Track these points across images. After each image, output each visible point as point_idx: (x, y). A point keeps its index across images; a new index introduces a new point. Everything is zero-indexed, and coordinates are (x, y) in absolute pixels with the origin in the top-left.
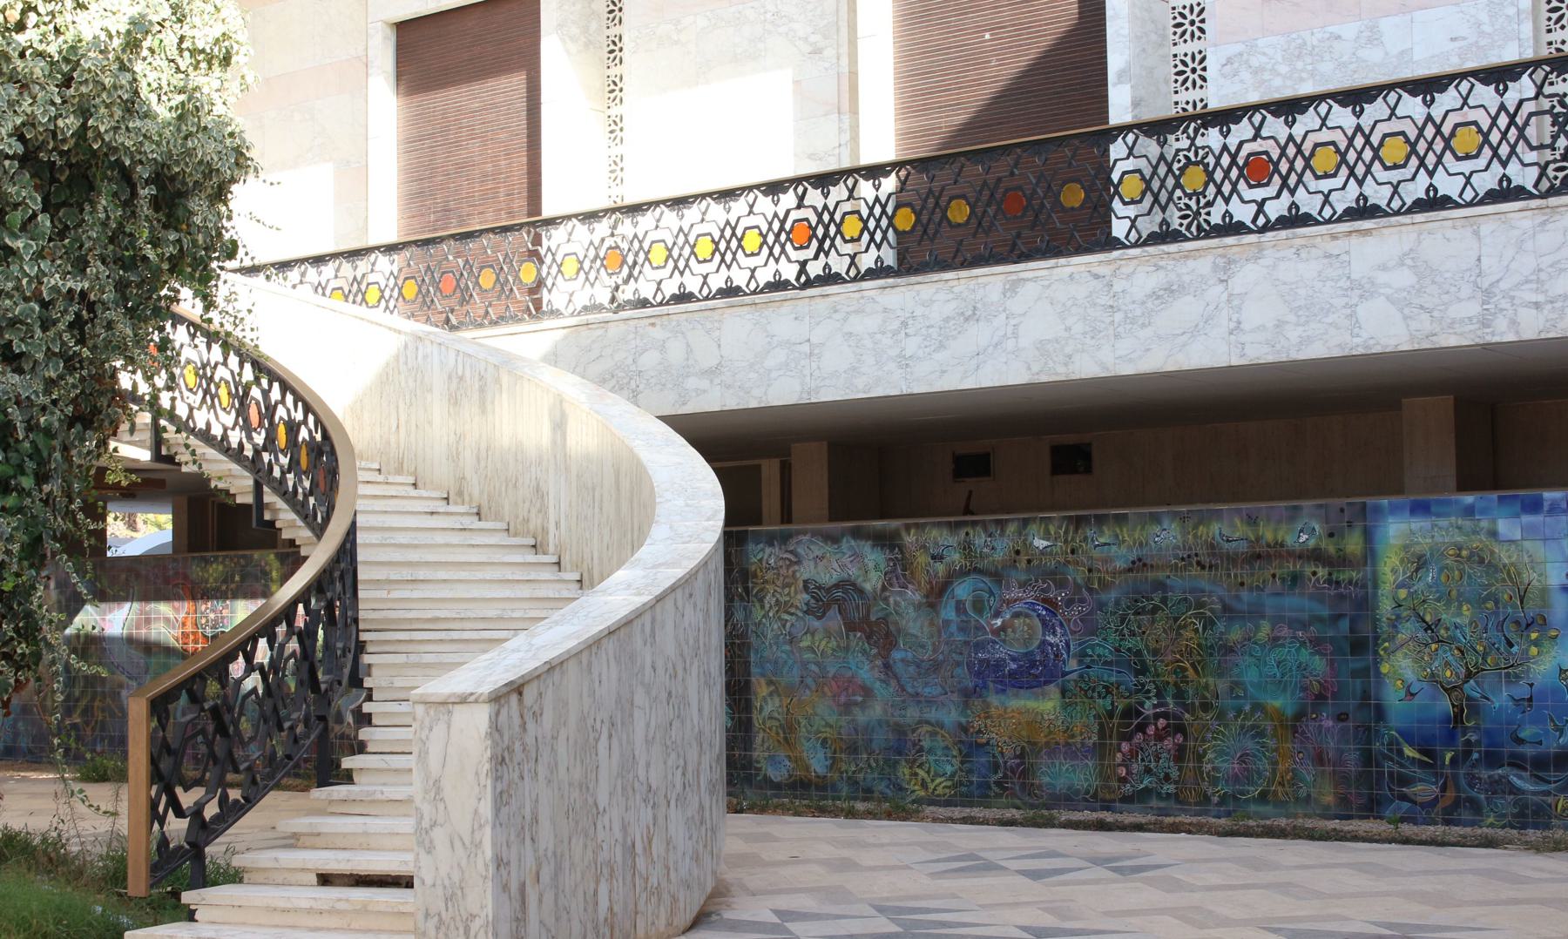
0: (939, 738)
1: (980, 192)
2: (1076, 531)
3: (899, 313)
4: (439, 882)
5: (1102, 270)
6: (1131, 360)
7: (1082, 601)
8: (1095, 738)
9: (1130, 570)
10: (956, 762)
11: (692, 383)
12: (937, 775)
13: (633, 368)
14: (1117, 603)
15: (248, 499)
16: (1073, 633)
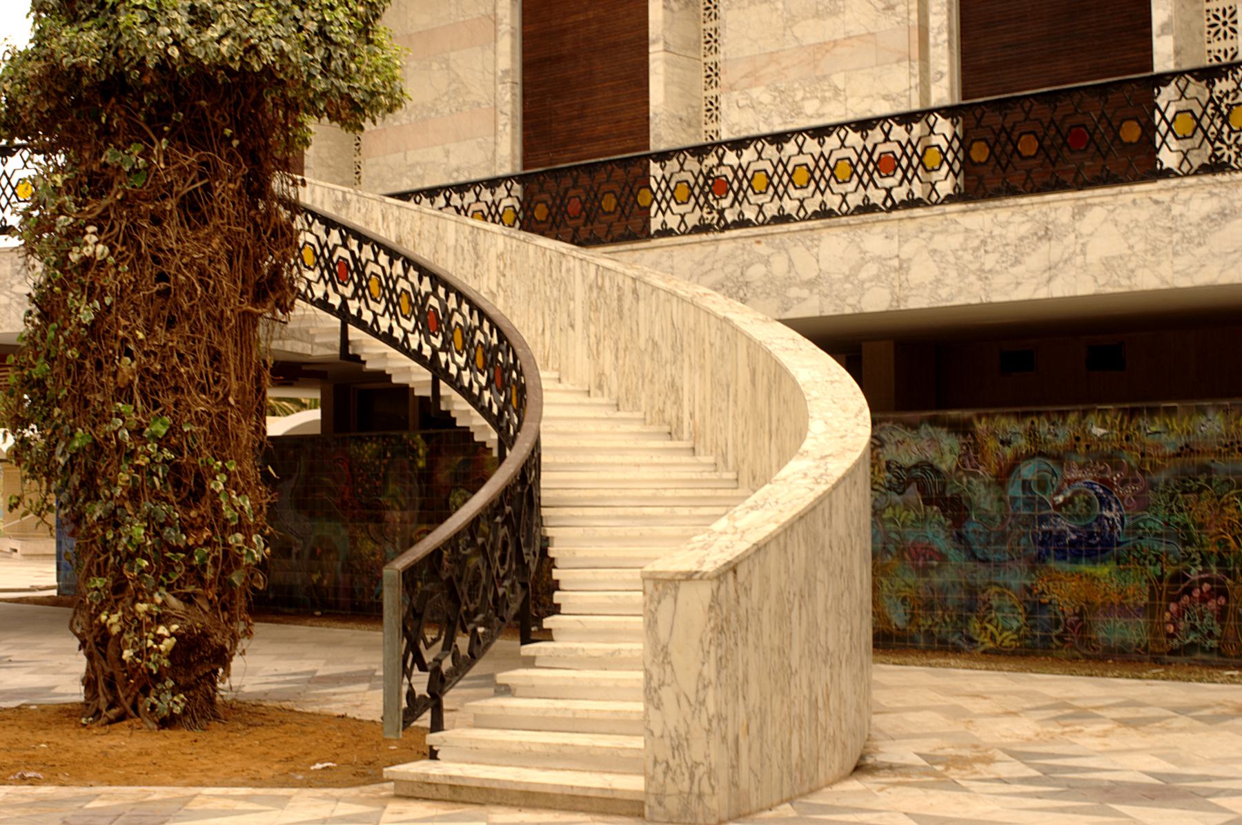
0: (1007, 598)
1: (1048, 128)
2: (1130, 421)
3: (980, 233)
4: (667, 733)
5: (1165, 197)
6: (1187, 275)
7: (1135, 481)
8: (1146, 599)
9: (1179, 455)
10: (1022, 619)
11: (794, 292)
12: (1004, 629)
13: (741, 279)
14: (1167, 483)
15: (428, 392)
16: (1127, 508)
